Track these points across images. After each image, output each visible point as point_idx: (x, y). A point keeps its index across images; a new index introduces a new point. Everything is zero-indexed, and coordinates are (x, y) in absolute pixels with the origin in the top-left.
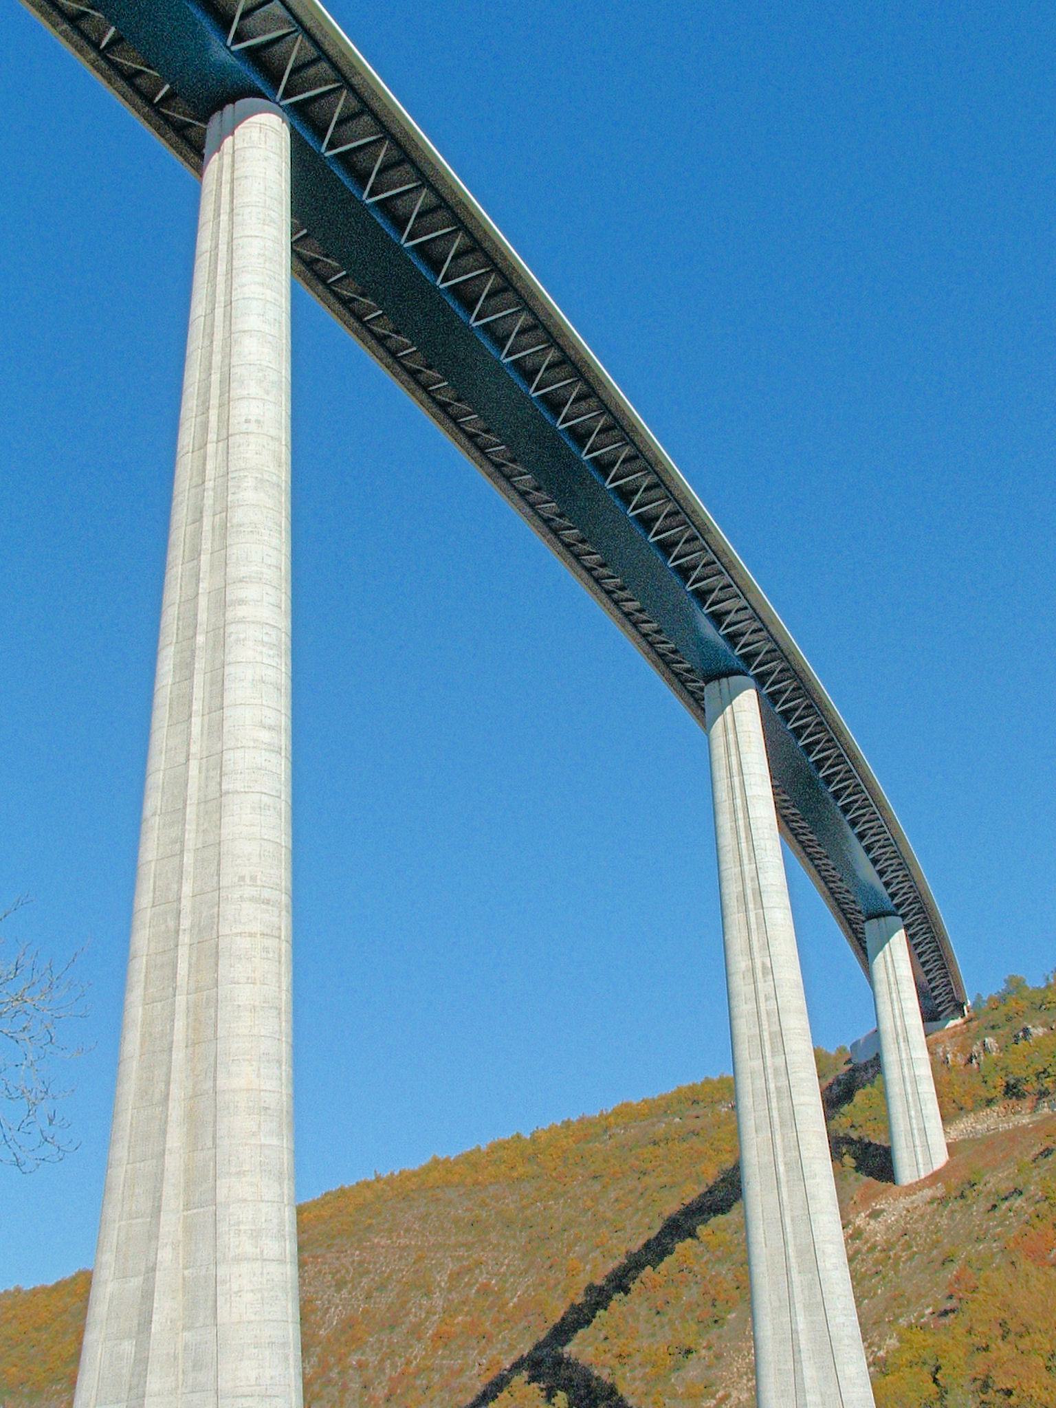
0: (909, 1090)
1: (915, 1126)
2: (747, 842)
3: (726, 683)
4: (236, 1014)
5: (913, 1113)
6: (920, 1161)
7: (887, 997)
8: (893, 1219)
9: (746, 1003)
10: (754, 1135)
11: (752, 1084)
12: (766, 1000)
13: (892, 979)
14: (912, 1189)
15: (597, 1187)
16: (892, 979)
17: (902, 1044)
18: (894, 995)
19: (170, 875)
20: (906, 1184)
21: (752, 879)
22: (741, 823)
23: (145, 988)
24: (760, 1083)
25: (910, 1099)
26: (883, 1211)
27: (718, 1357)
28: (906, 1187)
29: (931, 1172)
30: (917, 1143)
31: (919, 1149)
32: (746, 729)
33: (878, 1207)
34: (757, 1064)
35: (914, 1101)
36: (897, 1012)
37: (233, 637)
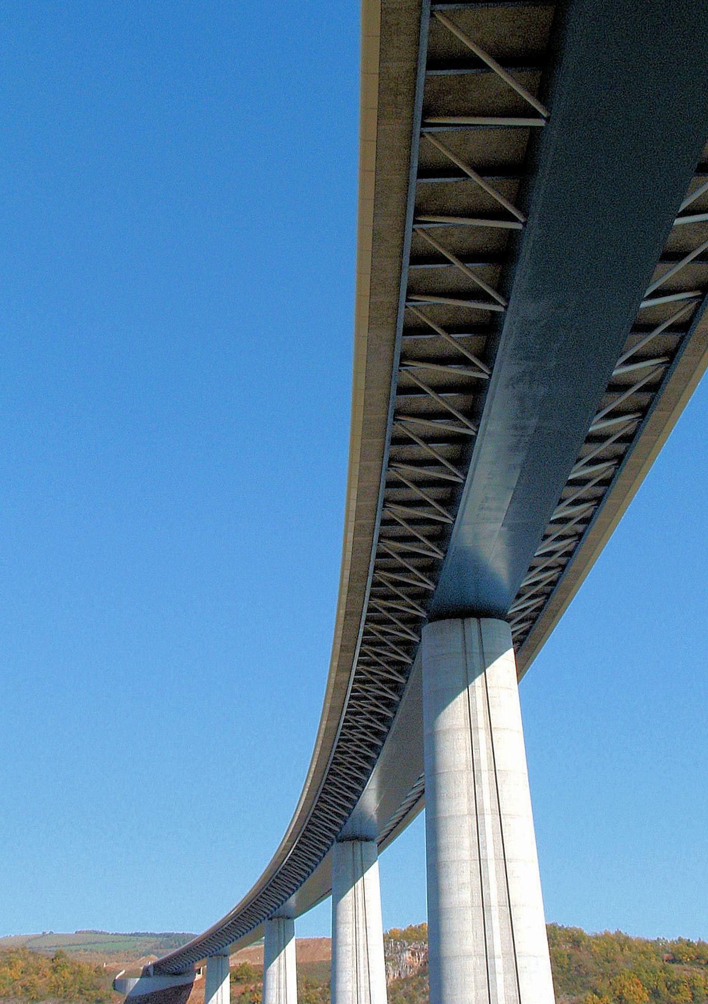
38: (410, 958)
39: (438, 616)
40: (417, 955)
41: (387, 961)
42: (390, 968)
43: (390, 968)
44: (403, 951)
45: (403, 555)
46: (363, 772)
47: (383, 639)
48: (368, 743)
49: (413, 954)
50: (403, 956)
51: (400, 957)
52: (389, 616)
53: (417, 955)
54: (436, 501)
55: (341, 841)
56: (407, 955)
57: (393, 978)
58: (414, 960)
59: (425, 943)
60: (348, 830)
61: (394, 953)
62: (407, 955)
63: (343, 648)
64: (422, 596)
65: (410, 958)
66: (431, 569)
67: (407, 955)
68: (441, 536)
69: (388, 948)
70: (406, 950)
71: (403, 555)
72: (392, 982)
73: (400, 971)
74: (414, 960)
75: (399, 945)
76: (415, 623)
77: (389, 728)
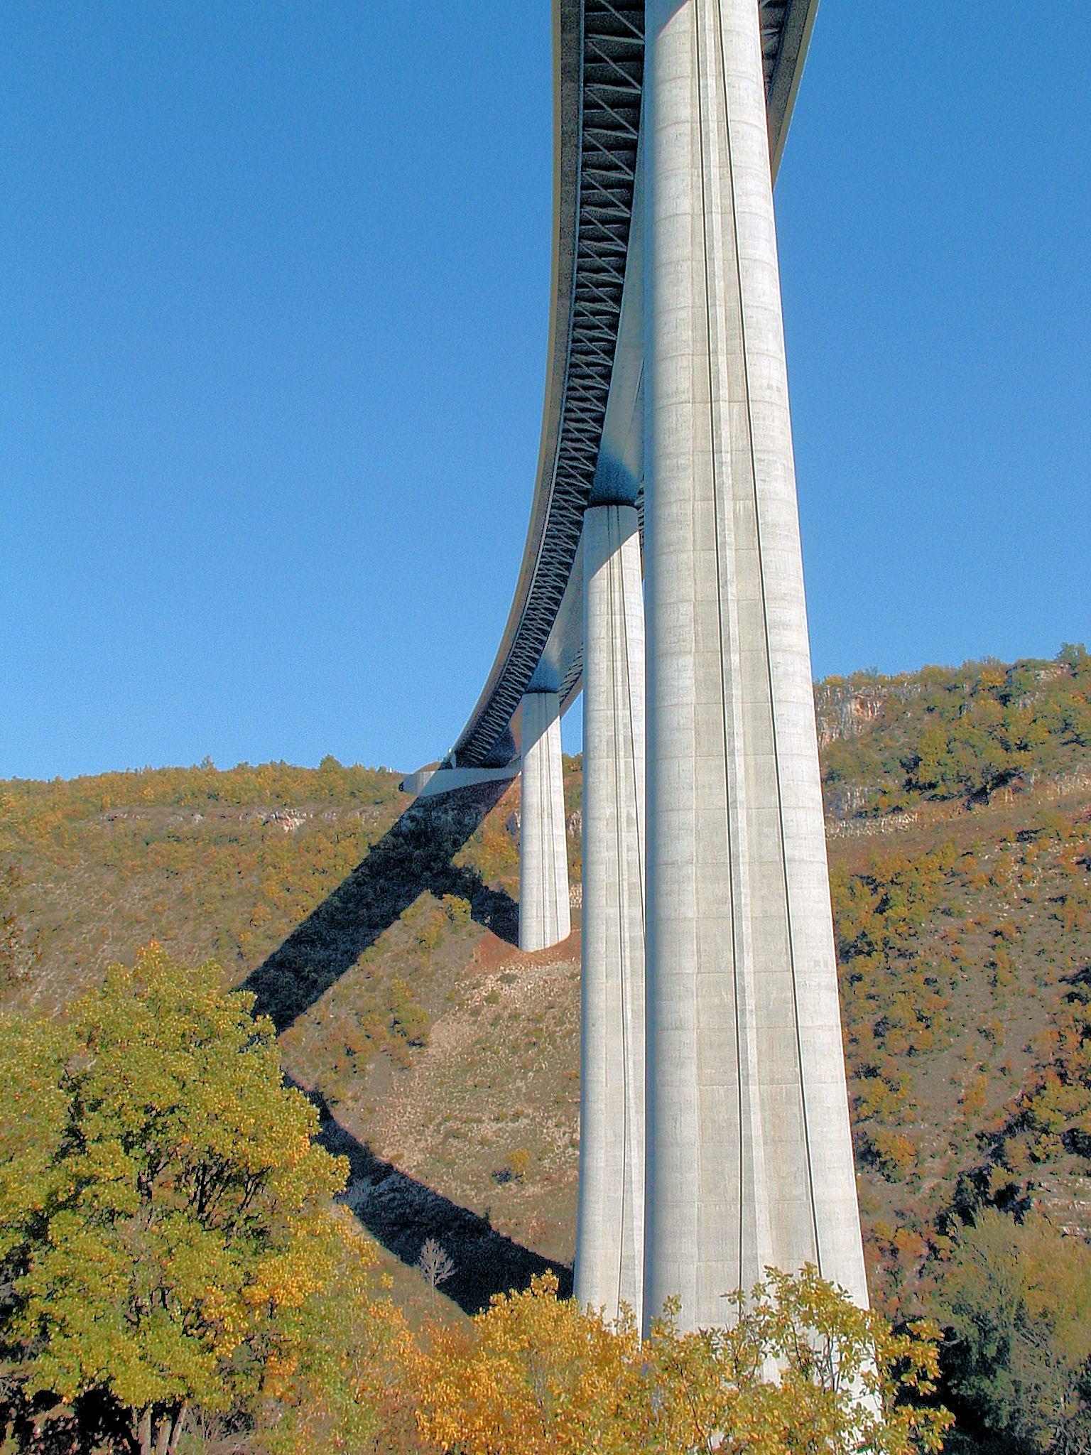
0: (547, 865)
1: (547, 898)
2: (623, 686)
3: (616, 510)
4: (827, 1117)
5: (547, 886)
6: (548, 931)
7: (537, 774)
8: (529, 987)
9: (607, 850)
10: (604, 980)
11: (607, 930)
12: (628, 851)
13: (545, 756)
14: (542, 957)
15: (111, 879)
16: (545, 756)
17: (546, 820)
18: (544, 772)
19: (719, 940)
20: (532, 951)
21: (625, 725)
22: (619, 664)
23: (699, 1068)
24: (615, 930)
25: (547, 873)
26: (515, 977)
27: (372, 1111)
28: (532, 954)
29: (556, 943)
30: (548, 914)
31: (548, 920)
32: (631, 566)
33: (508, 971)
34: (613, 912)
35: (549, 875)
36: (545, 788)
37: (781, 669)
38: (858, 711)
39: (595, 503)
40: (869, 706)
41: (820, 716)
42: (825, 725)
43: (825, 725)
44: (846, 700)
45: (576, 450)
46: (434, 1117)
47: (570, 489)
48: (593, 435)
49: (863, 704)
50: (846, 707)
51: (841, 709)
52: (572, 472)
53: (869, 706)
54: (587, 439)
55: (528, 692)
56: (853, 707)
57: (831, 740)
58: (866, 714)
59: (882, 687)
60: (533, 683)
61: (832, 705)
62: (853, 706)
63: (545, 473)
64: (585, 493)
65: (858, 711)
66: (589, 476)
67: (853, 706)
68: (596, 440)
69: (821, 698)
70: (852, 698)
71: (576, 450)
72: (827, 745)
73: (841, 731)
74: (866, 714)
75: (840, 691)
76: (581, 509)
77: (537, 665)
